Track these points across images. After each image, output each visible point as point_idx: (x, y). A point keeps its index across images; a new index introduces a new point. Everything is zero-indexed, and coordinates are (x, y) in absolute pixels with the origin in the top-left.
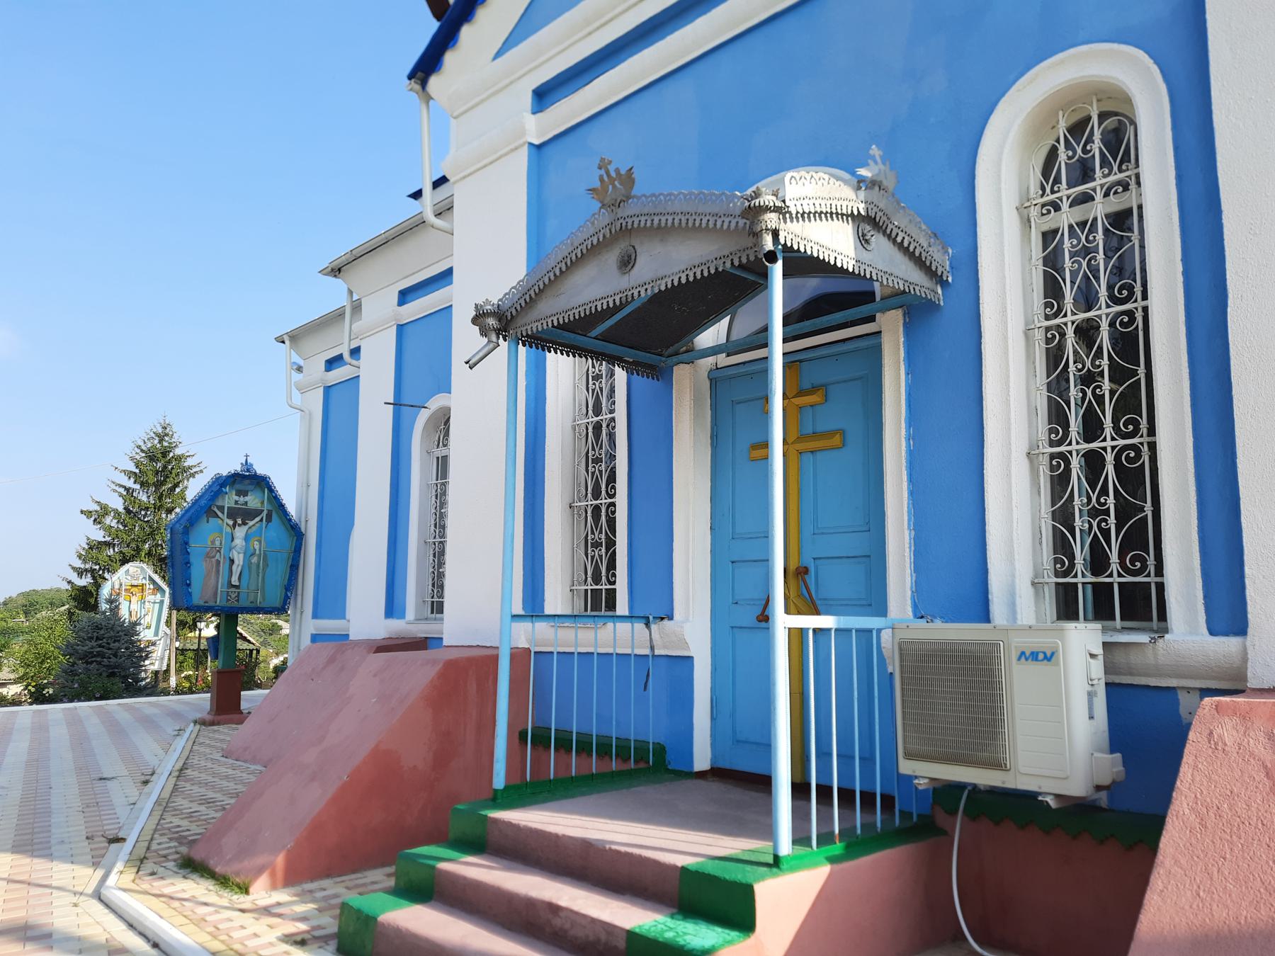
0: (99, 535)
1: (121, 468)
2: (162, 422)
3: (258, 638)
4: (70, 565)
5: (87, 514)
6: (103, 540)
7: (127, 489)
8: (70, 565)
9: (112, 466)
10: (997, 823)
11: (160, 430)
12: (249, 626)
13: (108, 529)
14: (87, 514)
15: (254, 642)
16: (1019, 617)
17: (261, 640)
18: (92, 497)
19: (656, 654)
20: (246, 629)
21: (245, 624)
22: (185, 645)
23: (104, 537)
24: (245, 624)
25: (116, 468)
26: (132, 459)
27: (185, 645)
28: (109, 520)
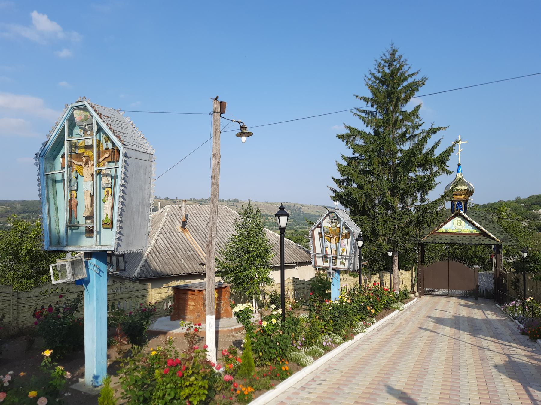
0: (349, 153)
1: (360, 96)
2: (390, 49)
3: (498, 235)
4: (333, 178)
5: (341, 137)
6: (353, 156)
7: (368, 113)
8: (333, 178)
9: (354, 95)
10: (484, 204)
11: (388, 57)
12: (491, 224)
13: (356, 148)
14: (341, 137)
15: (495, 238)
16: (102, 242)
17: (502, 236)
18: (345, 124)
19: (286, 217)
20: (488, 226)
21: (487, 223)
22: (434, 239)
23: (353, 154)
24: (487, 223)
25: (357, 96)
26: (371, 87)
27: (434, 239)
28: (359, 141)
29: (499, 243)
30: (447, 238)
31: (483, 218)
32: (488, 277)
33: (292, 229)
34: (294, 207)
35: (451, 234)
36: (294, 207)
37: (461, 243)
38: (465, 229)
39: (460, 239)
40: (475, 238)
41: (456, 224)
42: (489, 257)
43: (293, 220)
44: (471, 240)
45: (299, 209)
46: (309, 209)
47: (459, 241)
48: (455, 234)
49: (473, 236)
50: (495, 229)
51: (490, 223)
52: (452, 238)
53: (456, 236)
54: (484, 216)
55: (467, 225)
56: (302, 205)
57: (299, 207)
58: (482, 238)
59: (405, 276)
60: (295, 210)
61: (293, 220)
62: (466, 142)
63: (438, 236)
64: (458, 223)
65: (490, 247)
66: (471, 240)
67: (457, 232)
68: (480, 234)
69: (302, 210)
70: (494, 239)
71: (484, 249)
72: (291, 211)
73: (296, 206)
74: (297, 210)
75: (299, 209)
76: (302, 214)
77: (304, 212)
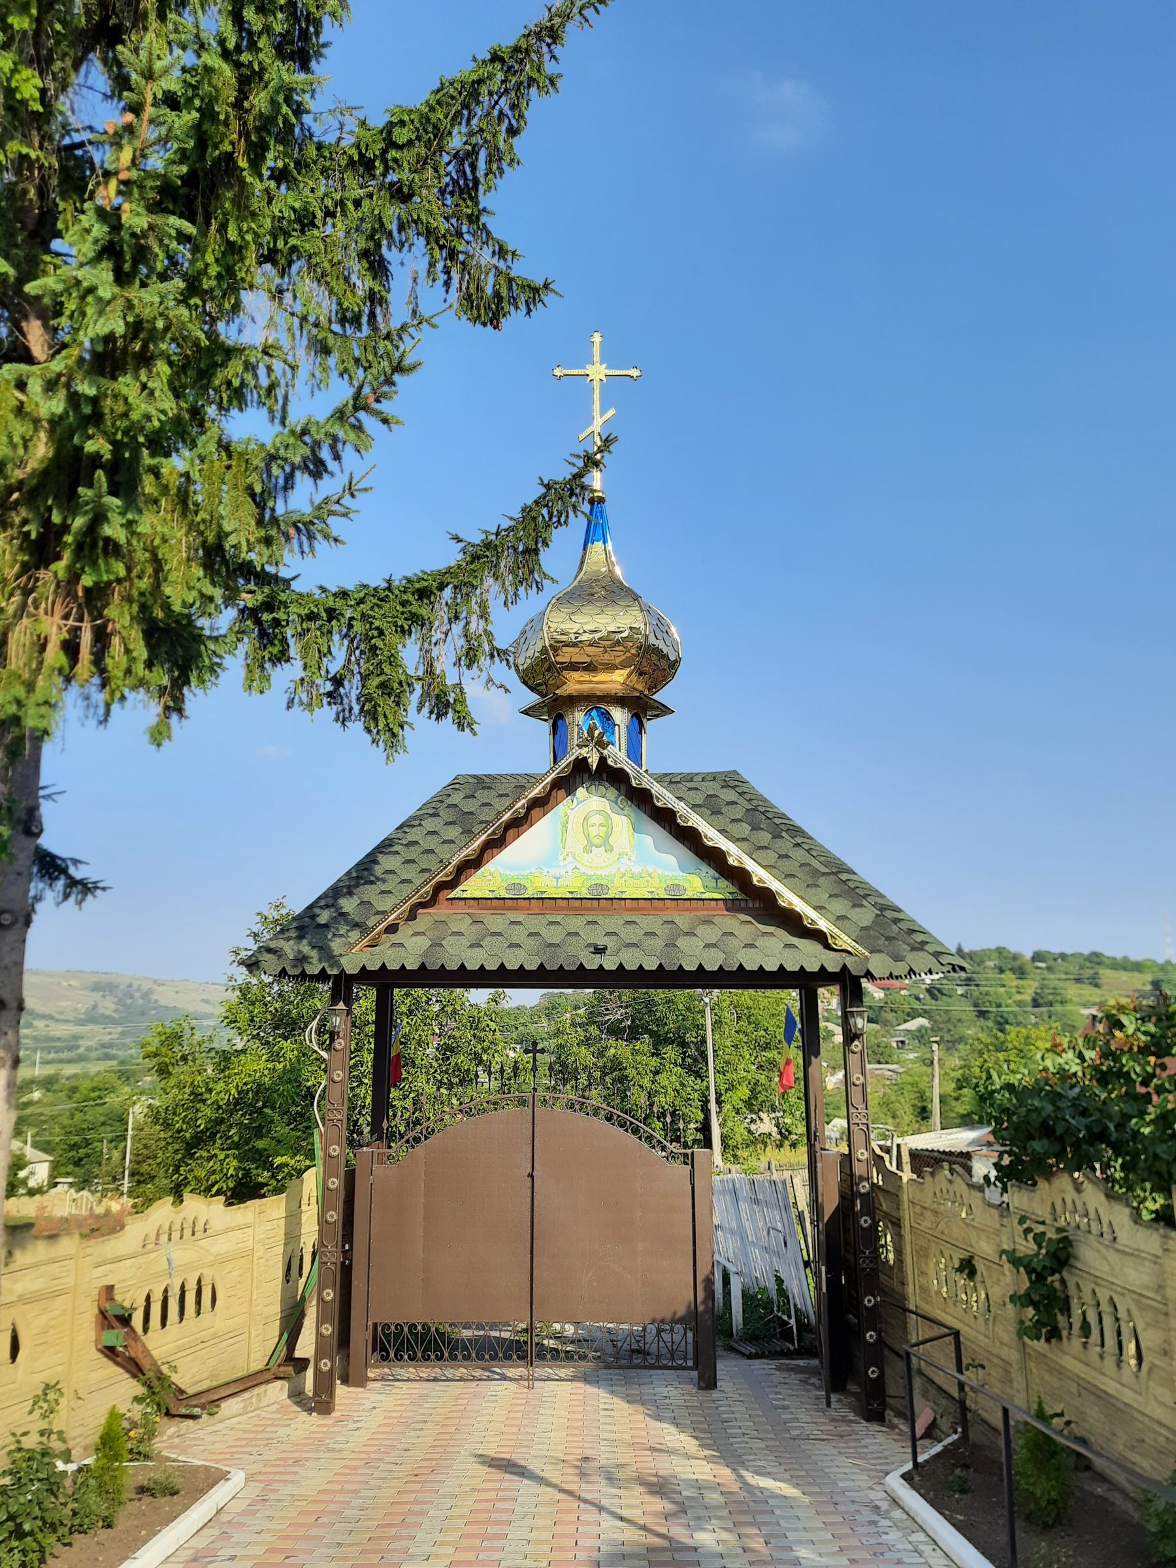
15: (823, 925)
21: (764, 837)
22: (437, 944)
27: (437, 944)
29: (849, 961)
30: (519, 935)
31: (738, 812)
32: (744, 1206)
33: (113, 1058)
34: (130, 985)
35: (545, 903)
36: (130, 985)
37: (610, 964)
38: (637, 870)
39: (601, 941)
40: (700, 930)
41: (576, 842)
42: (700, 1116)
43: (120, 1029)
44: (671, 945)
45: (146, 995)
46: (177, 992)
47: (600, 951)
48: (573, 904)
49: (682, 921)
50: (816, 873)
51: (778, 843)
52: (554, 935)
53: (576, 923)
54: (740, 800)
55: (648, 840)
56: (155, 982)
57: (146, 987)
58: (742, 927)
59: (221, 1246)
60: (132, 997)
61: (120, 1029)
62: (635, 373)
63: (464, 925)
64: (593, 831)
65: (700, 1077)
66: (671, 945)
67: (584, 894)
68: (732, 906)
69: (154, 997)
70: (818, 936)
71: (682, 1084)
72: (115, 1000)
73: (135, 984)
74: (137, 995)
75: (146, 995)
76: (155, 1008)
77: (163, 1002)
